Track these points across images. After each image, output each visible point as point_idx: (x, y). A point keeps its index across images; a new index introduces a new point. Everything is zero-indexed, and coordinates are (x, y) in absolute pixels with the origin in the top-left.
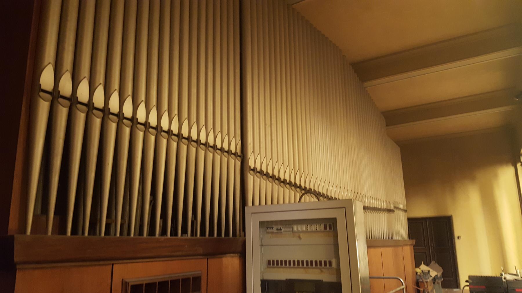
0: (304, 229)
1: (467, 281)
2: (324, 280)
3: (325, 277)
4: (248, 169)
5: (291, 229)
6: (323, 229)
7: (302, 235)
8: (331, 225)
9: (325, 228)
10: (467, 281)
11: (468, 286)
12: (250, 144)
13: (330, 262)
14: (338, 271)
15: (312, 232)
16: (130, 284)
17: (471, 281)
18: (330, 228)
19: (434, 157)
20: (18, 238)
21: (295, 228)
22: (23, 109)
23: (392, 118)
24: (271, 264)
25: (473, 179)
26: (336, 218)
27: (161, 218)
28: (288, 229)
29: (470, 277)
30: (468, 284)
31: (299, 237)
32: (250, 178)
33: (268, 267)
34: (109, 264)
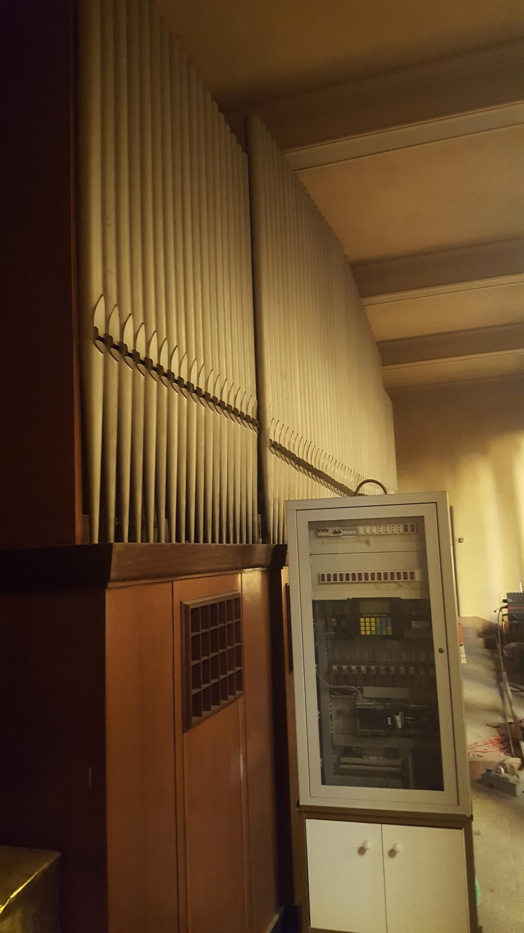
0: (368, 532)
1: (505, 601)
2: (403, 598)
3: (404, 592)
4: (268, 444)
5: (355, 532)
6: (402, 530)
7: (371, 540)
8: (414, 526)
9: (406, 530)
10: (505, 601)
11: (506, 607)
12: (270, 406)
13: (412, 574)
14: (425, 585)
15: (385, 535)
16: (191, 607)
17: (510, 600)
18: (412, 530)
19: (435, 415)
20: (118, 547)
21: (361, 530)
22: (75, 362)
23: (390, 352)
24: (324, 579)
25: (484, 452)
26: (422, 517)
27: (166, 518)
28: (352, 532)
29: (509, 595)
30: (506, 604)
31: (368, 542)
32: (273, 460)
33: (320, 584)
34: (169, 581)
